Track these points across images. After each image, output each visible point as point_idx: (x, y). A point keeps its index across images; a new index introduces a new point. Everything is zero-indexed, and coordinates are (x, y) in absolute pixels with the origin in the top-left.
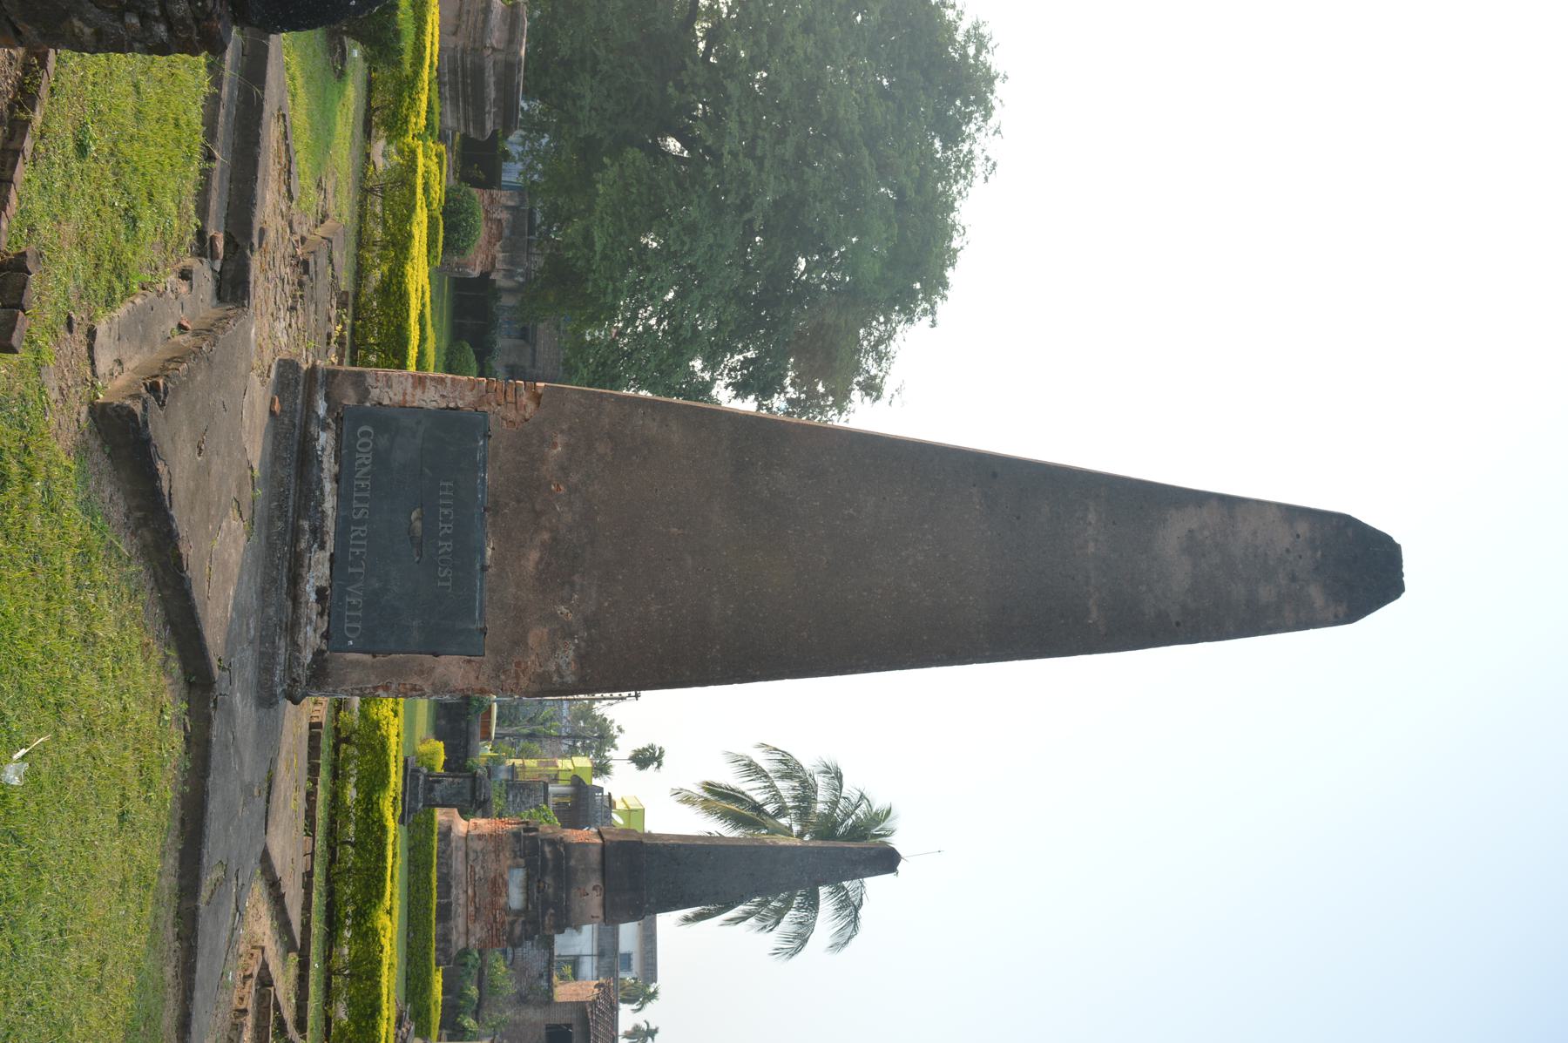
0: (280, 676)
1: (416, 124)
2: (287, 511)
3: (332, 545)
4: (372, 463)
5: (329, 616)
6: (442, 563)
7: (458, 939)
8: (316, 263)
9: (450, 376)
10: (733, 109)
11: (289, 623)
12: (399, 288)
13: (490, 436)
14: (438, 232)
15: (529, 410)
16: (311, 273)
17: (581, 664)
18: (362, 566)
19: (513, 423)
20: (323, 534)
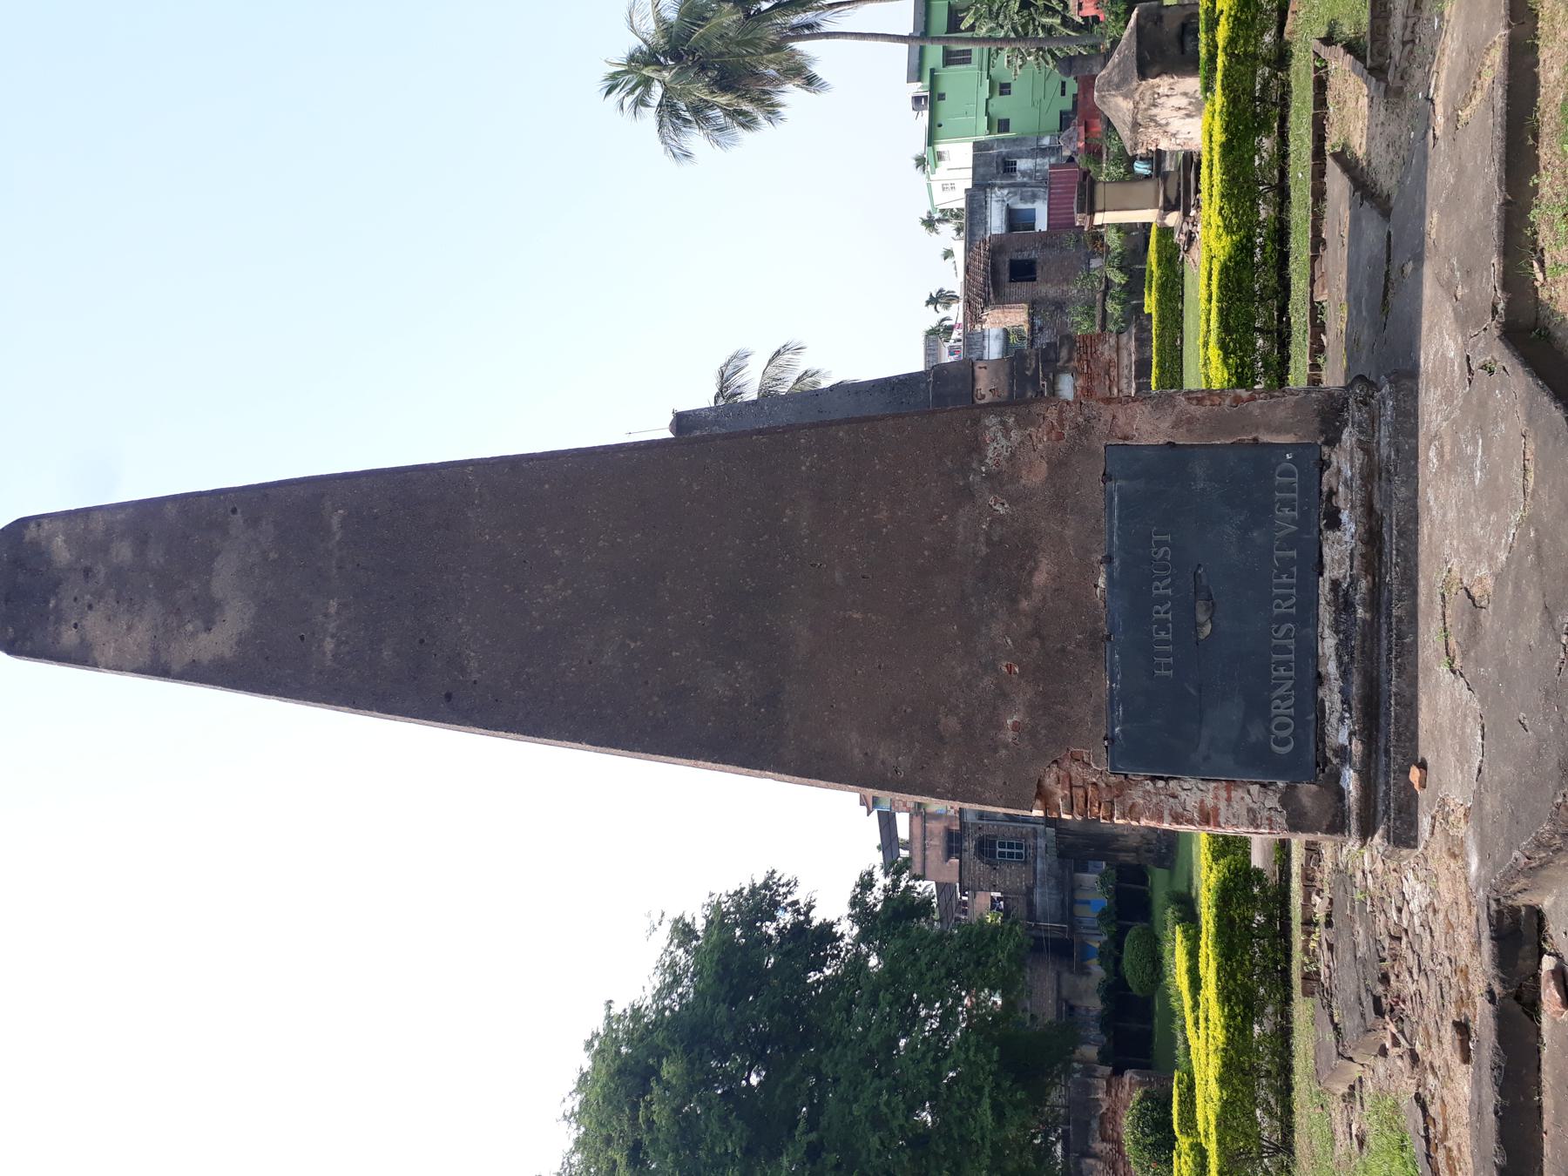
0: (1385, 408)
4: (1271, 702)
5: (1321, 491)
7: (1127, 343)
8: (1363, 1015)
9: (1166, 826)
12: (1231, 1009)
13: (1105, 739)
14: (1179, 1115)
16: (1370, 999)
19: (1075, 758)
20: (1334, 602)
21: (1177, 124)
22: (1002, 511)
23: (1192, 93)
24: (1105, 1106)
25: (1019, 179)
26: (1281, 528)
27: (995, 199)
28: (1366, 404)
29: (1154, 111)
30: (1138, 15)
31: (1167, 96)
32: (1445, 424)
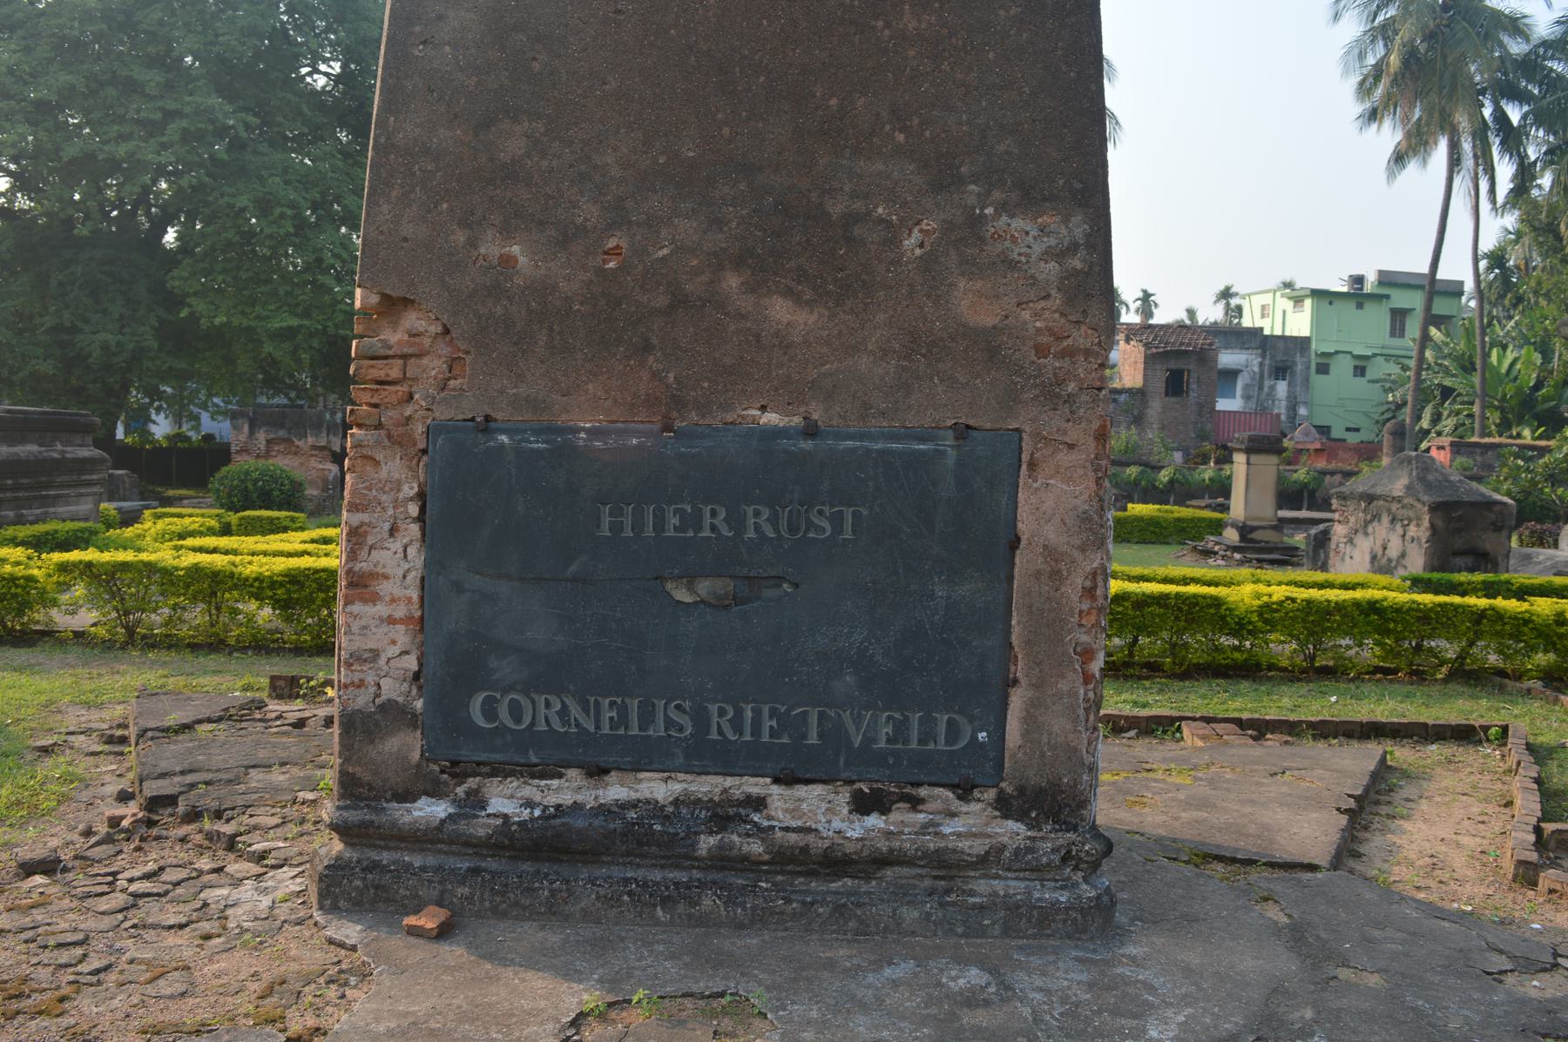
1: (18, 563)
2: (677, 884)
3: (752, 780)
5: (919, 785)
6: (798, 529)
10: (101, 150)
11: (935, 873)
12: (282, 584)
13: (488, 418)
15: (421, 325)
17: (1045, 199)
18: (805, 713)
20: (727, 800)
21: (1364, 546)
22: (909, 243)
23: (1404, 562)
24: (300, 443)
25: (1267, 383)
26: (857, 720)
27: (1250, 357)
28: (1064, 860)
29: (1386, 520)
30: (1505, 504)
31: (1404, 536)
32: (1026, 1012)
